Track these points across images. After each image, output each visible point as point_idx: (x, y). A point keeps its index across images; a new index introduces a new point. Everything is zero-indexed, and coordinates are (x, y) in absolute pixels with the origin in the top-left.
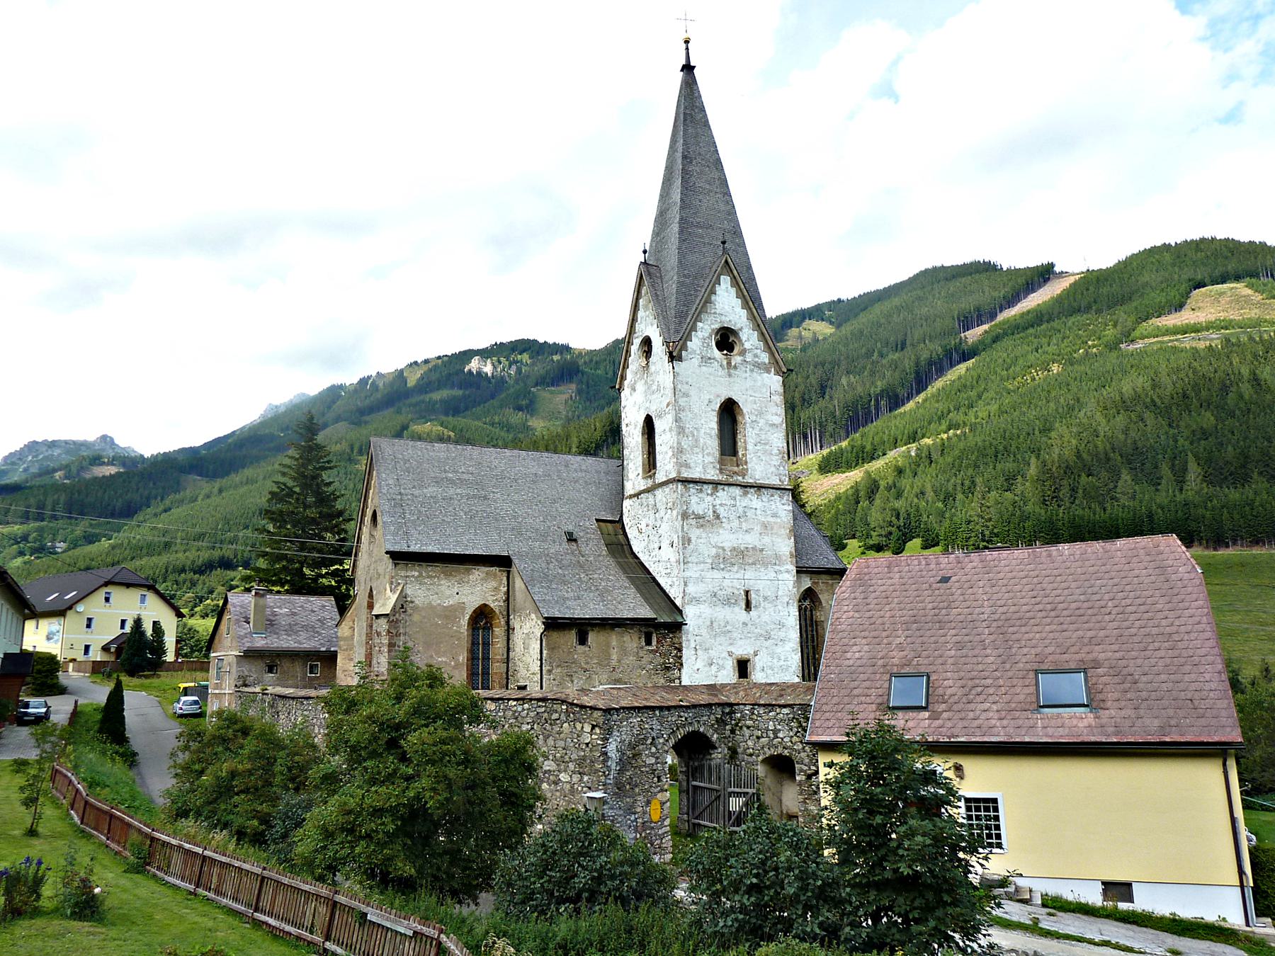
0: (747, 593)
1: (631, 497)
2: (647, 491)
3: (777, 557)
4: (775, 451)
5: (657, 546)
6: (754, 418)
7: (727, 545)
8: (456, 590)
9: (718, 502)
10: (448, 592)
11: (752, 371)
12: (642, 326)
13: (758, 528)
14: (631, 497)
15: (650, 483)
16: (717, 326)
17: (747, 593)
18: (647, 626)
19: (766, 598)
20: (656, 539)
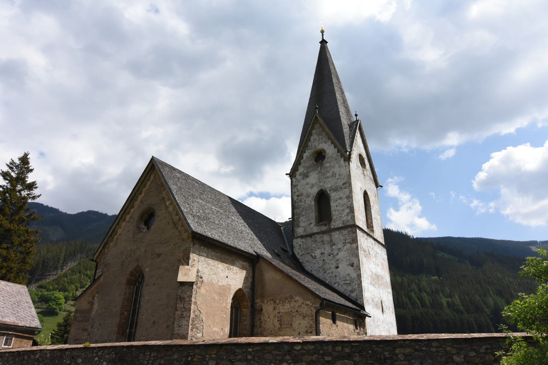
1: (302, 237)
2: (323, 233)
8: (226, 274)
12: (316, 144)
14: (302, 237)
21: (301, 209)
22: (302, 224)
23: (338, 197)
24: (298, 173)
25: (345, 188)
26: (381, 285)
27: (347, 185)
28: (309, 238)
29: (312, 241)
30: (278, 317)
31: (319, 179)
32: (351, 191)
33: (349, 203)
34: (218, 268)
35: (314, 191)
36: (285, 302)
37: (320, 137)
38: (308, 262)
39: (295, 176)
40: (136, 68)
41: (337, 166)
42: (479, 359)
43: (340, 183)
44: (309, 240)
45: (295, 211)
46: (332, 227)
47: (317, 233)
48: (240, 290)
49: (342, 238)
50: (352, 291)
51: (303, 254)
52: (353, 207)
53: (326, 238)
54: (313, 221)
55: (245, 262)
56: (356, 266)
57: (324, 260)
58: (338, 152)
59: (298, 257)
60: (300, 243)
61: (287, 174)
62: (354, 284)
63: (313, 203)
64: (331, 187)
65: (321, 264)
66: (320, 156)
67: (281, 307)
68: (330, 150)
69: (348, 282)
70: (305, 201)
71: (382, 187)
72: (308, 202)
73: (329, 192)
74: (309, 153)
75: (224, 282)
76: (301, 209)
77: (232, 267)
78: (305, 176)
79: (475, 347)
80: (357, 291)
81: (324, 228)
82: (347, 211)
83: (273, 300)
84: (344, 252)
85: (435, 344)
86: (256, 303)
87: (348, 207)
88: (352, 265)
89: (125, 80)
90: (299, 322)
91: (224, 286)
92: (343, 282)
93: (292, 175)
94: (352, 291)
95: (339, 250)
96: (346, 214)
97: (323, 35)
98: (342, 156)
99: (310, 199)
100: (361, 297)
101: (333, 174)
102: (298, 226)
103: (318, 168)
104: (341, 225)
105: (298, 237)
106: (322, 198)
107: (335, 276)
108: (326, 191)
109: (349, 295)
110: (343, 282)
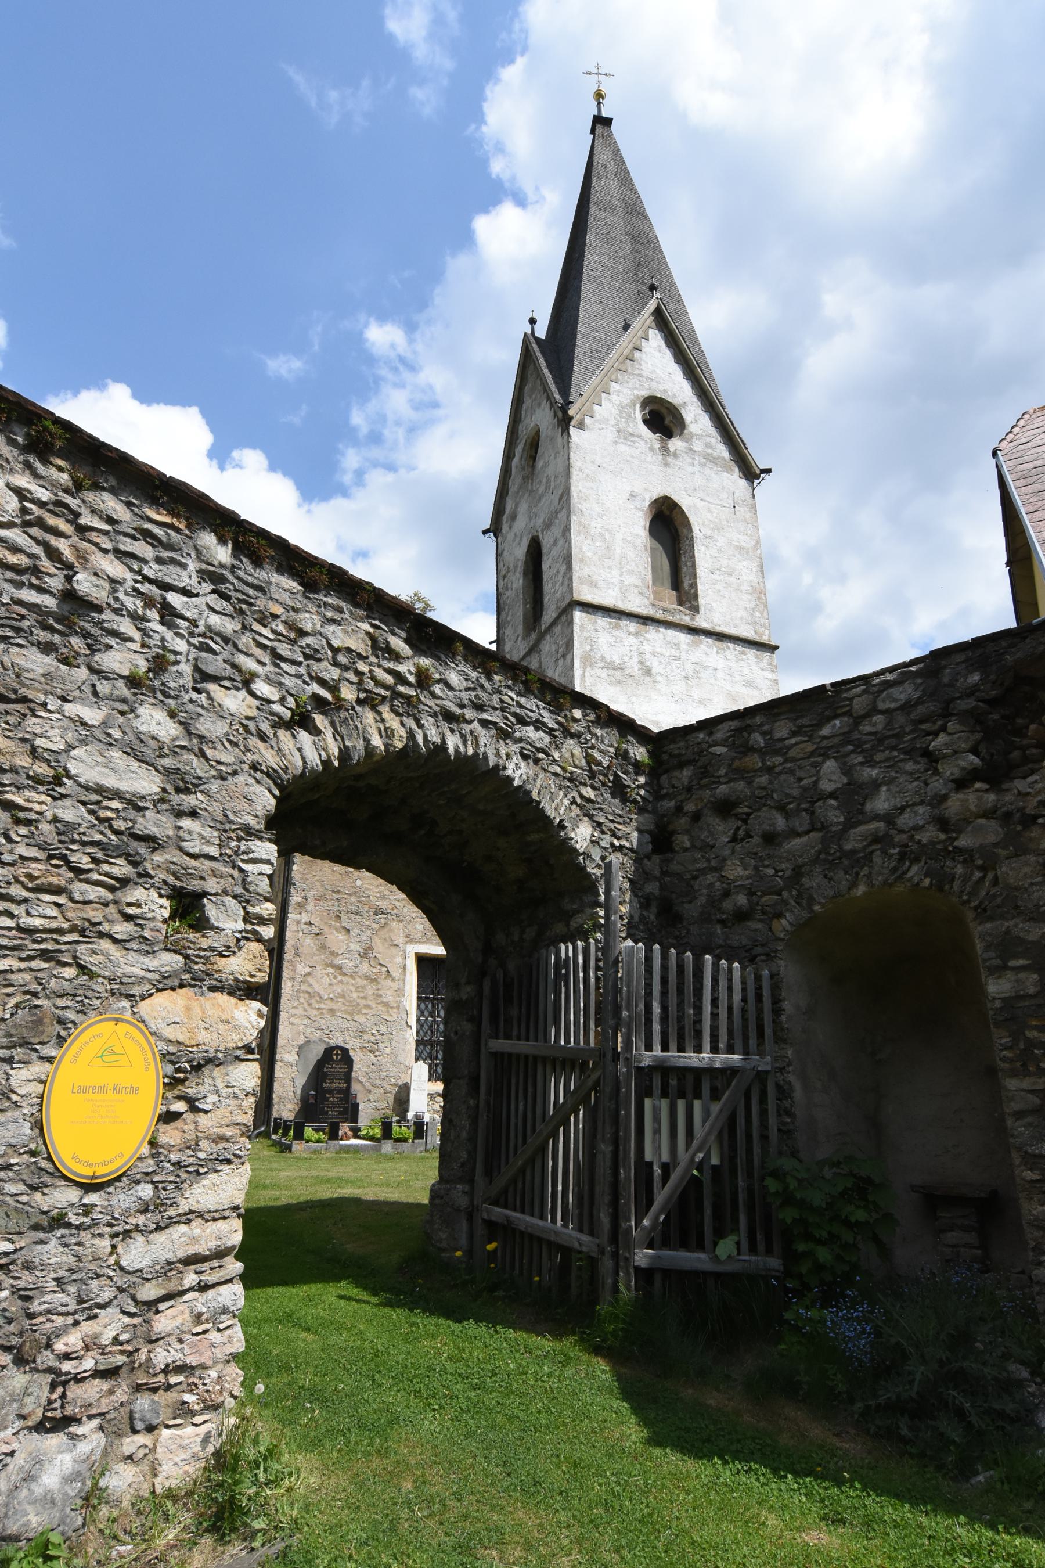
4: (746, 587)
6: (709, 533)
9: (647, 648)
11: (703, 465)
16: (645, 393)
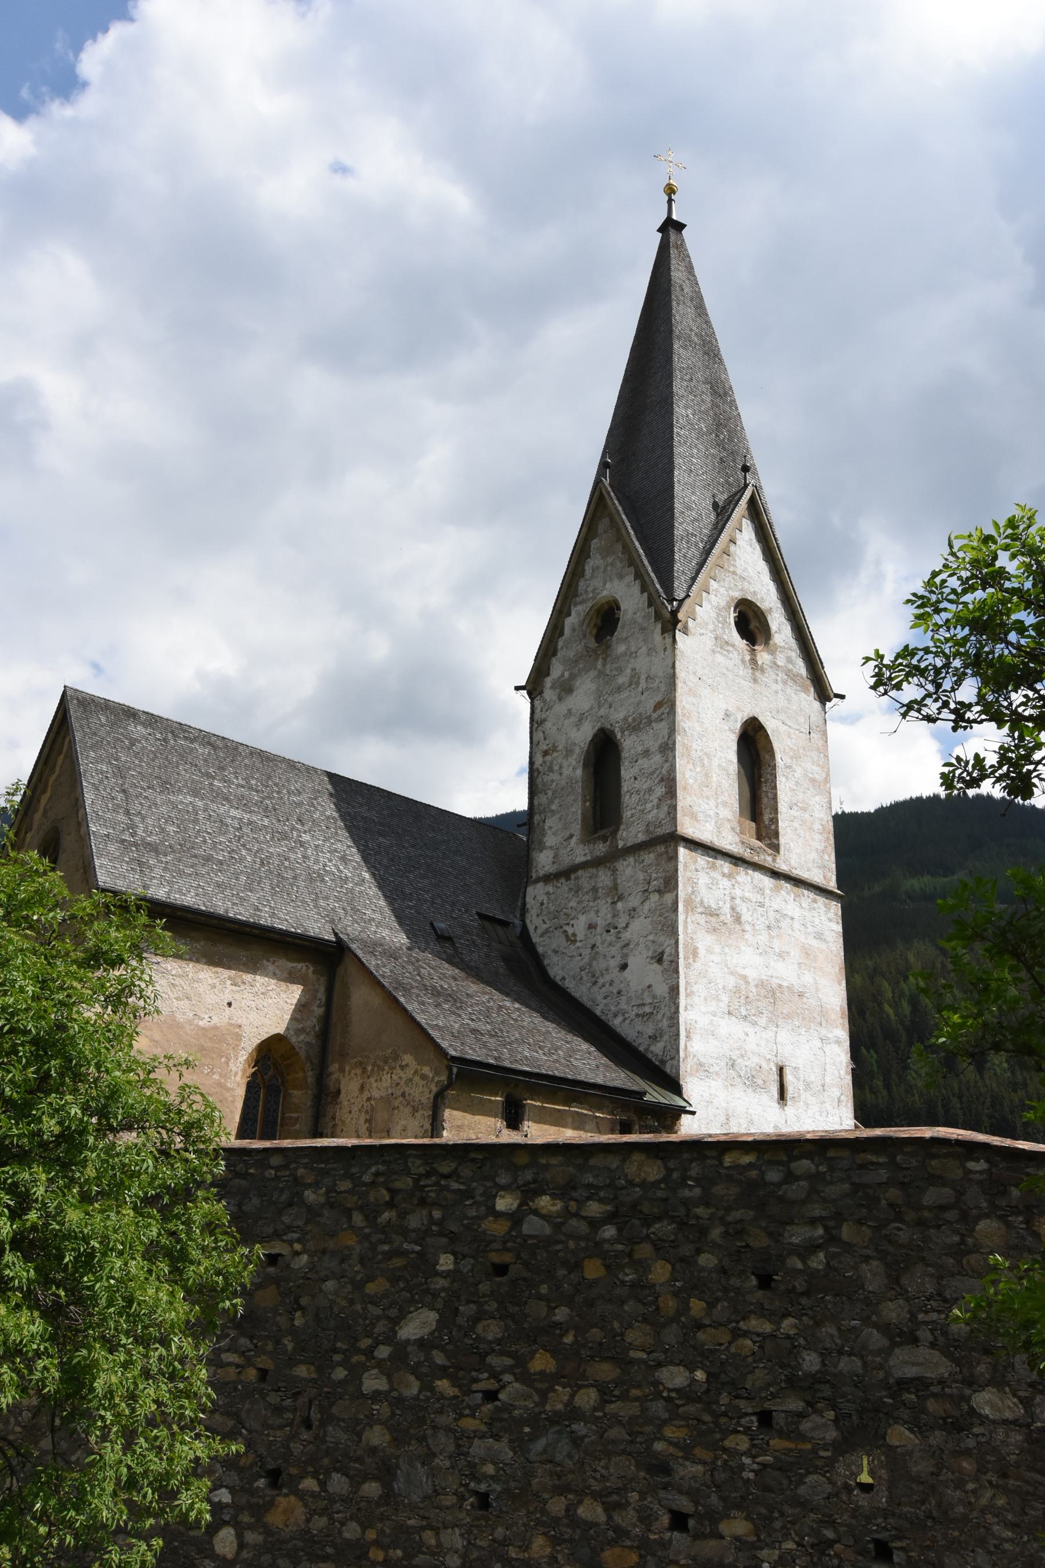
0: (781, 1070)
1: (547, 878)
2: (597, 863)
3: (823, 1012)
4: (817, 826)
5: (614, 963)
6: (789, 762)
7: (752, 974)
8: (228, 997)
9: (738, 892)
10: (210, 999)
12: (597, 583)
13: (795, 954)
14: (547, 878)
15: (601, 849)
16: (738, 595)
17: (781, 1070)
18: (625, 1107)
19: (808, 1086)
20: (614, 950)
21: (550, 793)
22: (550, 840)
23: (640, 749)
24: (548, 682)
25: (660, 719)
26: (788, 1017)
27: (665, 709)
28: (563, 880)
29: (570, 889)
30: (367, 1112)
31: (599, 694)
32: (672, 730)
33: (667, 765)
34: (199, 981)
35: (583, 735)
36: (383, 1070)
37: (610, 560)
38: (556, 952)
39: (541, 693)
40: (339, 348)
41: (644, 649)
42: (355, 1198)
43: (648, 704)
44: (564, 885)
45: (536, 803)
46: (621, 844)
47: (584, 866)
48: (276, 1038)
49: (641, 876)
50: (653, 1038)
51: (547, 931)
52: (673, 780)
53: (604, 878)
54: (576, 828)
55: (299, 961)
56: (667, 961)
57: (593, 946)
58: (650, 605)
59: (535, 939)
60: (540, 899)
61: (517, 688)
62: (659, 1016)
63: (579, 772)
64: (625, 719)
65: (586, 959)
66: (607, 619)
67: (374, 1085)
68: (631, 601)
69: (647, 1009)
70: (561, 767)
71: (842, 697)
72: (567, 772)
73: (619, 736)
74: (579, 614)
75: (220, 1018)
76: (550, 793)
77: (248, 977)
78: (566, 688)
79: (354, 1170)
80: (666, 1037)
81: (601, 849)
82: (660, 791)
83: (361, 1063)
84: (642, 919)
85: (276, 1160)
86: (331, 1073)
87: (662, 780)
88: (660, 961)
89: (315, 392)
90: (403, 1122)
91: (215, 1028)
92: (635, 1010)
93: (533, 687)
94: (653, 1038)
95: (632, 912)
96: (656, 801)
97: (670, 201)
98: (658, 616)
99: (573, 760)
100: (673, 1053)
101: (632, 677)
102: (542, 847)
103: (596, 660)
104: (641, 837)
105: (538, 880)
106: (604, 754)
107: (619, 993)
108: (613, 732)
109: (647, 1050)
110: (635, 1010)
